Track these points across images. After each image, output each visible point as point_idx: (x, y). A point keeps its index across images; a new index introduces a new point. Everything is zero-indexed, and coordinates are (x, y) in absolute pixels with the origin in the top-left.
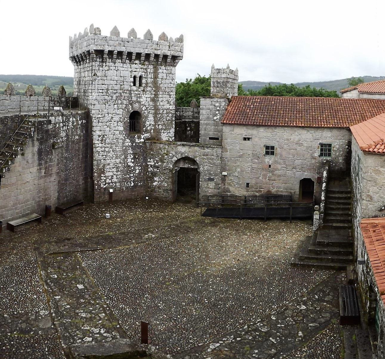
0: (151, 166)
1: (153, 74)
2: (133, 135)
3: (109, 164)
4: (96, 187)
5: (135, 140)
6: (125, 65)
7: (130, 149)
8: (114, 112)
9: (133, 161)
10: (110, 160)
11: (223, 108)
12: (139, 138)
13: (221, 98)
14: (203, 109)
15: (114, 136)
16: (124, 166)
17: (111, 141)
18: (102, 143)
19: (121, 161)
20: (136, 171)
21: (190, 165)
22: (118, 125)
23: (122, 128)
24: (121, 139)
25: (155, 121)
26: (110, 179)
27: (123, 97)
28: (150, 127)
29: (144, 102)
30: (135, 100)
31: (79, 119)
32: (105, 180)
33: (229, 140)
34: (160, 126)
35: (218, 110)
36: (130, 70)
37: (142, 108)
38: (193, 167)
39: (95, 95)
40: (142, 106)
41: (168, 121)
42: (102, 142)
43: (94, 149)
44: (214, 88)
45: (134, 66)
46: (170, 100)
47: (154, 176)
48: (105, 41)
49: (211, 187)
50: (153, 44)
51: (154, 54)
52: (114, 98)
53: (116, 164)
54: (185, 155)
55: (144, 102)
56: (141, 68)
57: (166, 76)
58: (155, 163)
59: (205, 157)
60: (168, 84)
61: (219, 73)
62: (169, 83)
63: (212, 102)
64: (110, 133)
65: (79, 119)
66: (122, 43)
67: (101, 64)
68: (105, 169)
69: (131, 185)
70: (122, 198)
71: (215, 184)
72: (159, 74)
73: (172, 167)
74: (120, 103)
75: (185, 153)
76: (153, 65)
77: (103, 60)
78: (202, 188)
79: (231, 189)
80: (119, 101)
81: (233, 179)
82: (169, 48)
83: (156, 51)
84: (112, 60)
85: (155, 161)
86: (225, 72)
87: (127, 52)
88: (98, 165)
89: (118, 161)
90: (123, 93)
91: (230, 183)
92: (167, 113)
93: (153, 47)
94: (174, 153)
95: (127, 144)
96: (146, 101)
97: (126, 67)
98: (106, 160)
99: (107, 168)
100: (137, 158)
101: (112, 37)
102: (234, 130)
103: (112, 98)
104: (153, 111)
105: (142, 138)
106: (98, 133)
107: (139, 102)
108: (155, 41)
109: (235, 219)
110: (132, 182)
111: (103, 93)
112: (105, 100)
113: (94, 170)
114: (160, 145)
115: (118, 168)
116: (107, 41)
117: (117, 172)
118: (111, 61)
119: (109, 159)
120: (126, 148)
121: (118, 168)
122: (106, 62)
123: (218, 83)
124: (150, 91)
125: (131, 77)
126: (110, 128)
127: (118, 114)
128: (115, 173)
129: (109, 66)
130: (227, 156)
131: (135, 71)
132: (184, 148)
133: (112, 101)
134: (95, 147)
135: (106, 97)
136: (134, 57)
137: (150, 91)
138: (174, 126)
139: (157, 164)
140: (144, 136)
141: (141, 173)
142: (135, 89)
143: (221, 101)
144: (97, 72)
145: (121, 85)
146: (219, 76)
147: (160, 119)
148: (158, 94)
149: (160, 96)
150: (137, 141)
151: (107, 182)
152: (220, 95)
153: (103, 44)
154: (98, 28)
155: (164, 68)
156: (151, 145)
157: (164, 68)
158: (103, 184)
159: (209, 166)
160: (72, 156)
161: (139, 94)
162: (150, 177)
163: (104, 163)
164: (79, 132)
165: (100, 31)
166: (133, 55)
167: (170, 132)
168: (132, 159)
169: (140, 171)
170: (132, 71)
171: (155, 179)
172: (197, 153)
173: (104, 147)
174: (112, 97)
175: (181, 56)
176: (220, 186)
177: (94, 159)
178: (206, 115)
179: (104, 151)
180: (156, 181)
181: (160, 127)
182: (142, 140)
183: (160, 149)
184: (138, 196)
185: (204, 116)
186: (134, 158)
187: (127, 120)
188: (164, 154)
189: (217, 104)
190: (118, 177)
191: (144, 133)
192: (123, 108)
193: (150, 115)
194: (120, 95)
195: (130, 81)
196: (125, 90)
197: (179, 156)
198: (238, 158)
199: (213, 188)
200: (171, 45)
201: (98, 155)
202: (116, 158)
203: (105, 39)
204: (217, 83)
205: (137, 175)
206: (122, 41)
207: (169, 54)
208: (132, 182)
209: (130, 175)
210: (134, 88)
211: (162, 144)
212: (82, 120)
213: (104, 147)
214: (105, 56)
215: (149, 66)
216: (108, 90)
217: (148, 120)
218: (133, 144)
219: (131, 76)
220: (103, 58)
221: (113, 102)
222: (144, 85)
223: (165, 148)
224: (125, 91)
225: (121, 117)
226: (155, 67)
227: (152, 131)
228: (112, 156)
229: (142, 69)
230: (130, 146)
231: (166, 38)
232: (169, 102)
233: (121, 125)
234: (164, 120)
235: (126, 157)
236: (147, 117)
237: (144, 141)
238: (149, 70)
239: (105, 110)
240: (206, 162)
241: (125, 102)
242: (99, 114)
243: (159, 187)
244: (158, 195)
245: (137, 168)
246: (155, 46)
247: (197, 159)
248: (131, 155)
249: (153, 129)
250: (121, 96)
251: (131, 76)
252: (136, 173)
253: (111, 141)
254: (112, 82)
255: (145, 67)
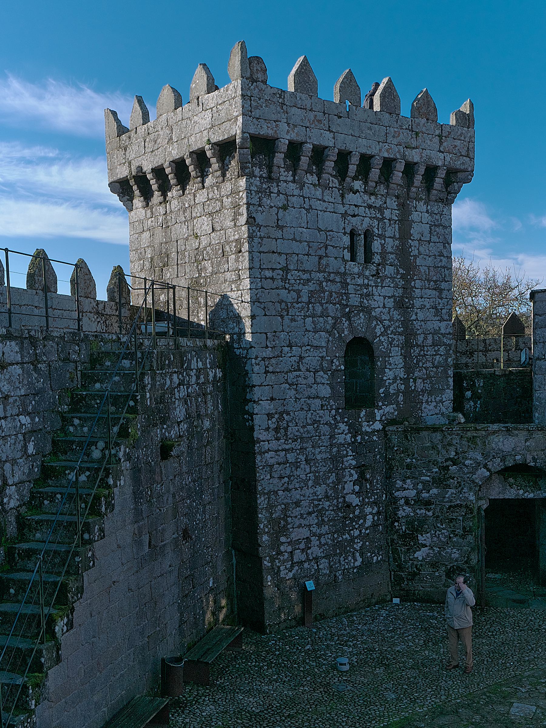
0: (407, 503)
1: (397, 226)
7: (350, 453)
8: (305, 340)
10: (302, 488)
12: (371, 418)
16: (337, 506)
17: (302, 430)
18: (278, 439)
21: (521, 492)
23: (325, 391)
25: (409, 369)
30: (357, 304)
34: (419, 381)
36: (342, 210)
38: (531, 496)
40: (375, 323)
43: (258, 458)
47: (417, 531)
53: (316, 502)
57: (430, 233)
58: (419, 493)
64: (298, 406)
68: (289, 519)
72: (414, 225)
74: (319, 314)
77: (270, 172)
80: (316, 308)
82: (441, 143)
85: (420, 486)
87: (336, 151)
89: (320, 490)
90: (327, 282)
92: (434, 345)
94: (480, 458)
95: (341, 439)
96: (384, 307)
97: (332, 200)
105: (378, 418)
106: (266, 406)
107: (367, 310)
110: (358, 554)
111: (276, 282)
115: (321, 512)
117: (319, 525)
118: (290, 178)
125: (345, 233)
129: (286, 194)
132: (511, 439)
134: (262, 453)
139: (425, 495)
141: (378, 525)
142: (356, 270)
145: (321, 258)
147: (418, 363)
150: (366, 428)
153: (274, 117)
157: (424, 208)
158: (286, 568)
163: (286, 501)
167: (442, 401)
169: (376, 518)
171: (421, 539)
173: (283, 450)
174: (298, 292)
175: (469, 170)
177: (260, 488)
180: (425, 546)
181: (420, 385)
182: (378, 426)
186: (361, 479)
187: (339, 365)
190: (323, 541)
192: (328, 327)
194: (318, 288)
197: (496, 465)
201: (269, 477)
202: (317, 483)
205: (368, 532)
206: (324, 113)
207: (440, 164)
213: (283, 450)
216: (286, 269)
217: (390, 364)
220: (270, 167)
222: (377, 259)
230: (349, 444)
233: (323, 381)
237: (381, 427)
238: (387, 213)
242: (267, 347)
243: (434, 565)
245: (368, 510)
249: (402, 392)
254: (296, 247)
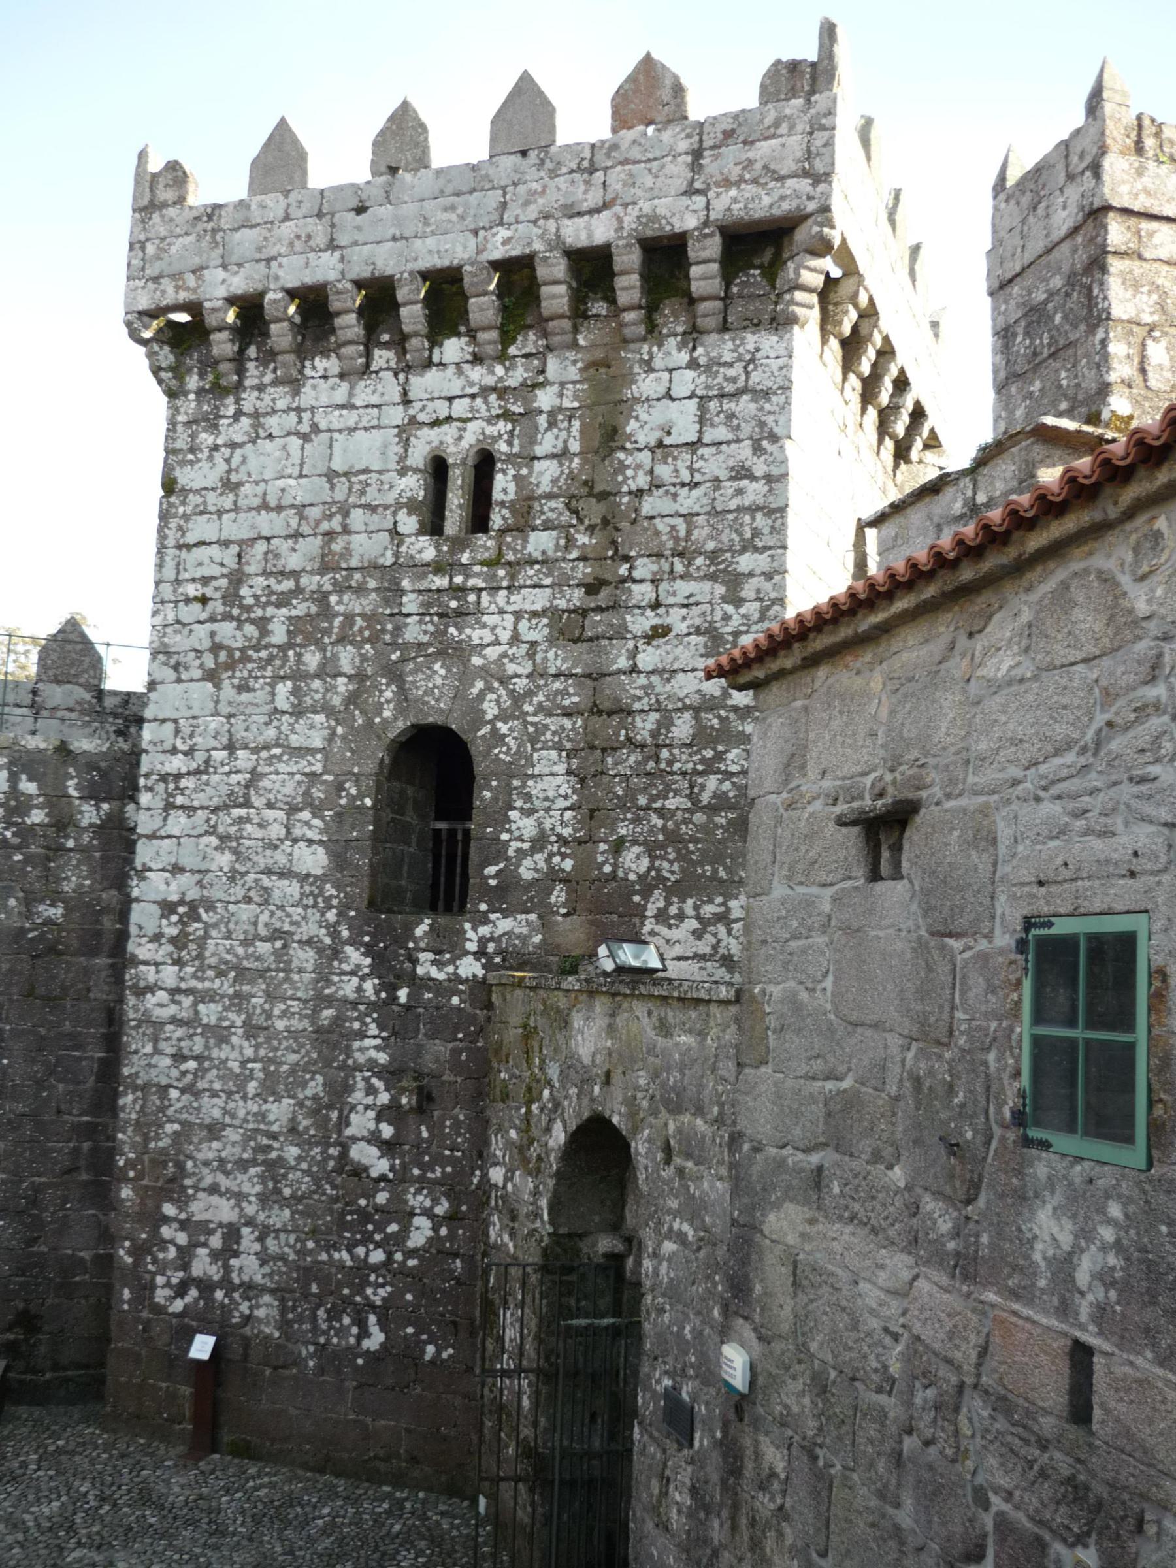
3: (214, 1131)
4: (127, 1294)
5: (415, 961)
7: (373, 1029)
9: (387, 1131)
10: (229, 1094)
17: (240, 951)
18: (178, 962)
20: (405, 1230)
22: (297, 832)
23: (314, 860)
27: (337, 622)
28: (540, 858)
29: (499, 650)
37: (481, 696)
40: (480, 685)
43: (131, 1000)
46: (736, 621)
55: (499, 650)
56: (485, 391)
62: (723, 474)
64: (238, 892)
65: (73, 792)
69: (367, 1344)
83: (580, 221)
88: (147, 1126)
89: (279, 1111)
93: (552, 199)
95: (348, 987)
96: (515, 639)
97: (375, 400)
99: (200, 1156)
103: (264, 632)
110: (372, 1319)
111: (211, 604)
115: (274, 1169)
120: (338, 1021)
121: (274, 1169)
126: (236, 852)
133: (264, 654)
140: (484, 930)
142: (430, 554)
147: (631, 793)
149: (642, 592)
155: (684, 357)
168: (378, 1119)
170: (413, 421)
174: (262, 624)
175: (811, 207)
192: (336, 701)
194: (314, 609)
201: (149, 1049)
202: (269, 1089)
205: (412, 1263)
208: (372, 1319)
216: (237, 578)
218: (392, 989)
222: (497, 519)
225: (318, 768)
231: (665, 94)
233: (310, 834)
235: (339, 1092)
236: (519, 769)
241: (347, 658)
245: (418, 1200)
250: (326, 612)
252: (411, 1244)
253: (240, 951)
254: (267, 523)
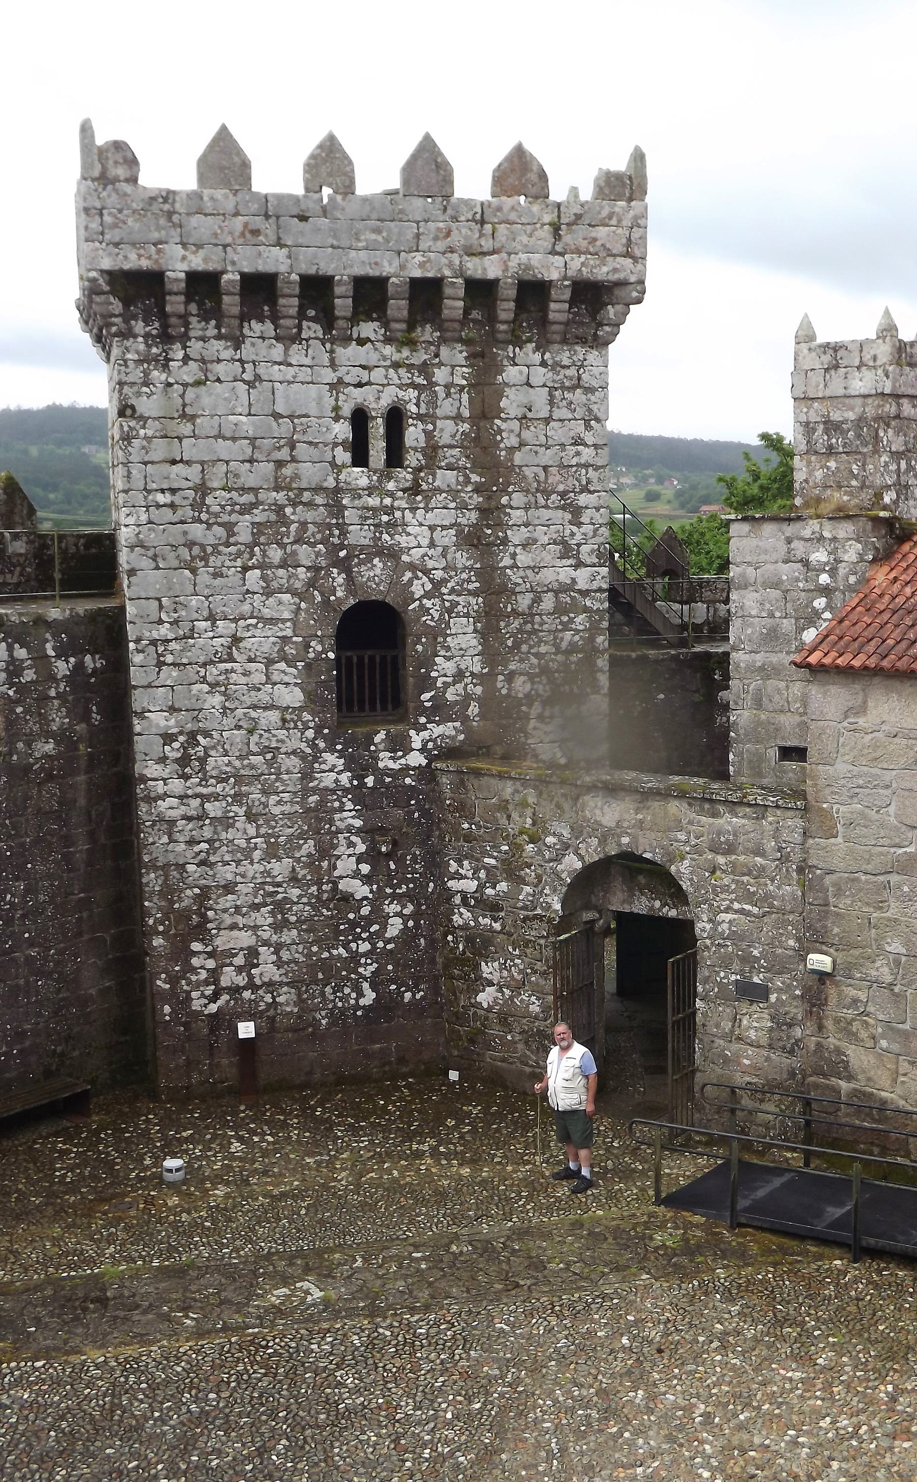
0: (465, 902)
1: (465, 397)
2: (361, 730)
3: (229, 888)
5: (377, 759)
6: (297, 354)
7: (349, 806)
8: (246, 608)
9: (365, 868)
10: (238, 862)
11: (852, 579)
12: (399, 745)
13: (841, 515)
14: (746, 587)
15: (254, 738)
17: (237, 763)
18: (186, 777)
19: (301, 873)
21: (657, 904)
22: (276, 677)
23: (294, 697)
24: (294, 753)
26: (239, 970)
27: (293, 527)
28: (459, 687)
30: (366, 542)
31: (51, 653)
32: (215, 975)
33: (841, 767)
34: (519, 681)
35: (826, 591)
36: (329, 376)
37: (410, 582)
38: (673, 913)
39: (131, 520)
40: (408, 575)
41: (568, 652)
42: (188, 770)
43: (143, 807)
44: (809, 463)
45: (349, 353)
46: (578, 537)
47: (481, 955)
48: (162, 221)
49: (752, 1034)
50: (455, 219)
51: (460, 281)
52: (244, 534)
54: (620, 845)
55: (421, 551)
56: (396, 365)
58: (481, 887)
59: (721, 860)
60: (563, 445)
61: (836, 367)
63: (789, 541)
65: (51, 653)
66: (268, 228)
67: (154, 350)
68: (210, 914)
69: (362, 1002)
70: (310, 1073)
71: (772, 1019)
73: (558, 906)
75: (620, 836)
76: (467, 342)
77: (165, 326)
78: (706, 1039)
79: (856, 1056)
80: (271, 553)
81: (863, 996)
83: (476, 260)
84: (218, 327)
85: (482, 874)
86: (867, 357)
87: (295, 277)
88: (169, 892)
89: (280, 868)
91: (850, 1023)
92: (559, 610)
93: (457, 239)
94: (566, 833)
95: (328, 780)
96: (432, 545)
97: (307, 361)
98: (212, 865)
100: (389, 856)
101: (207, 193)
102: (870, 704)
103: (231, 533)
104: (473, 601)
105: (417, 744)
106: (160, 720)
107: (392, 554)
108: (468, 203)
109: (827, 1251)
110: (365, 985)
111: (180, 512)
112: (190, 545)
113: (151, 922)
114: (500, 784)
115: (280, 907)
116: (175, 218)
117: (277, 927)
119: (227, 858)
120: (322, 802)
121: (280, 907)
122: (184, 339)
123: (831, 427)
124: (453, 493)
125: (337, 419)
126: (224, 694)
127: (272, 621)
128: (265, 936)
129: (203, 361)
130: (836, 862)
131: (360, 385)
133: (232, 549)
135: (197, 531)
136: (343, 305)
137: (453, 493)
138: (603, 680)
140: (425, 734)
141: (415, 937)
142: (364, 482)
143: (841, 534)
144: (139, 394)
145: (280, 464)
146: (836, 387)
147: (517, 645)
148: (501, 508)
149: (517, 516)
150: (386, 761)
151: (225, 982)
152: (840, 497)
153: (156, 235)
154: (119, 146)
155: (537, 357)
156: (462, 782)
158: (203, 996)
159: (741, 911)
160: (22, 845)
161: (390, 510)
162: (462, 961)
164: (58, 719)
165: (132, 162)
166: (338, 290)
169: (411, 923)
172: (682, 836)
173: (197, 796)
174: (230, 528)
175: (633, 279)
176: (798, 1032)
177: (146, 858)
178: (765, 621)
179: (199, 818)
181: (521, 686)
182: (416, 759)
183: (503, 806)
184: (402, 1060)
185: (751, 625)
186: (372, 856)
188: (521, 833)
189: (819, 556)
190: (285, 955)
191: (423, 720)
193: (459, 624)
194: (273, 517)
195: (330, 437)
196: (302, 490)
197: (592, 850)
198: (894, 878)
199: (764, 1041)
200: (564, 220)
201: (165, 839)
202: (272, 853)
203: (166, 207)
204: (826, 431)
205: (389, 947)
206: (267, 216)
207: (554, 275)
208: (365, 985)
209: (353, 945)
210: (359, 477)
211: (509, 783)
212: (79, 652)
213: (197, 796)
214: (175, 304)
215: (444, 351)
216: (203, 489)
217: (448, 649)
218: (361, 778)
219: (336, 409)
221: (239, 554)
222: (413, 459)
223: (524, 804)
224: (307, 496)
225: (289, 632)
226: (482, 355)
227: (473, 709)
228: (243, 843)
229: (402, 371)
232: (567, 550)
233: (286, 679)
234: (543, 649)
235: (325, 851)
236: (437, 634)
238: (441, 375)
239: (194, 601)
240: (725, 889)
241: (305, 554)
243: (504, 1019)
244: (503, 1060)
245: (392, 908)
246: (463, 234)
247: (682, 870)
248: (354, 839)
249: (479, 700)
250: (285, 521)
251: (336, 409)
253: (237, 763)
254: (223, 448)
255: (421, 357)
